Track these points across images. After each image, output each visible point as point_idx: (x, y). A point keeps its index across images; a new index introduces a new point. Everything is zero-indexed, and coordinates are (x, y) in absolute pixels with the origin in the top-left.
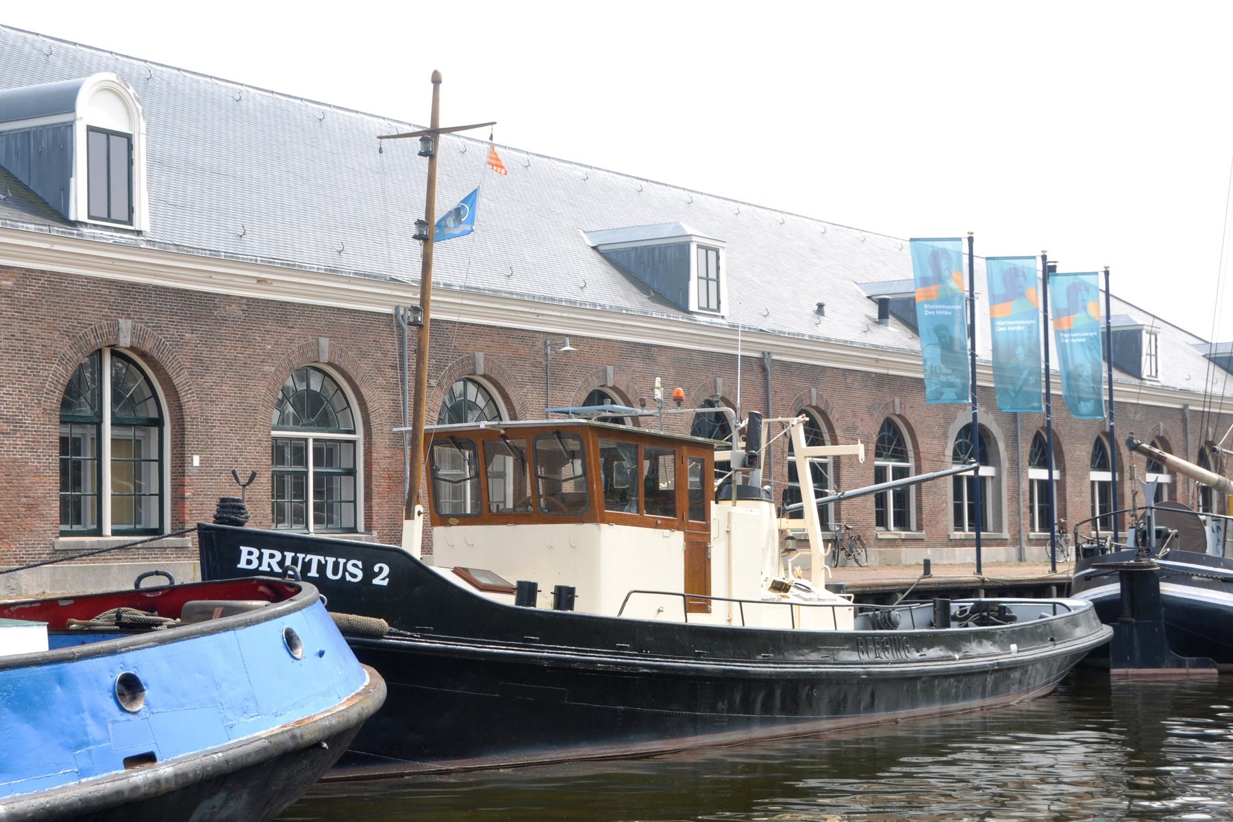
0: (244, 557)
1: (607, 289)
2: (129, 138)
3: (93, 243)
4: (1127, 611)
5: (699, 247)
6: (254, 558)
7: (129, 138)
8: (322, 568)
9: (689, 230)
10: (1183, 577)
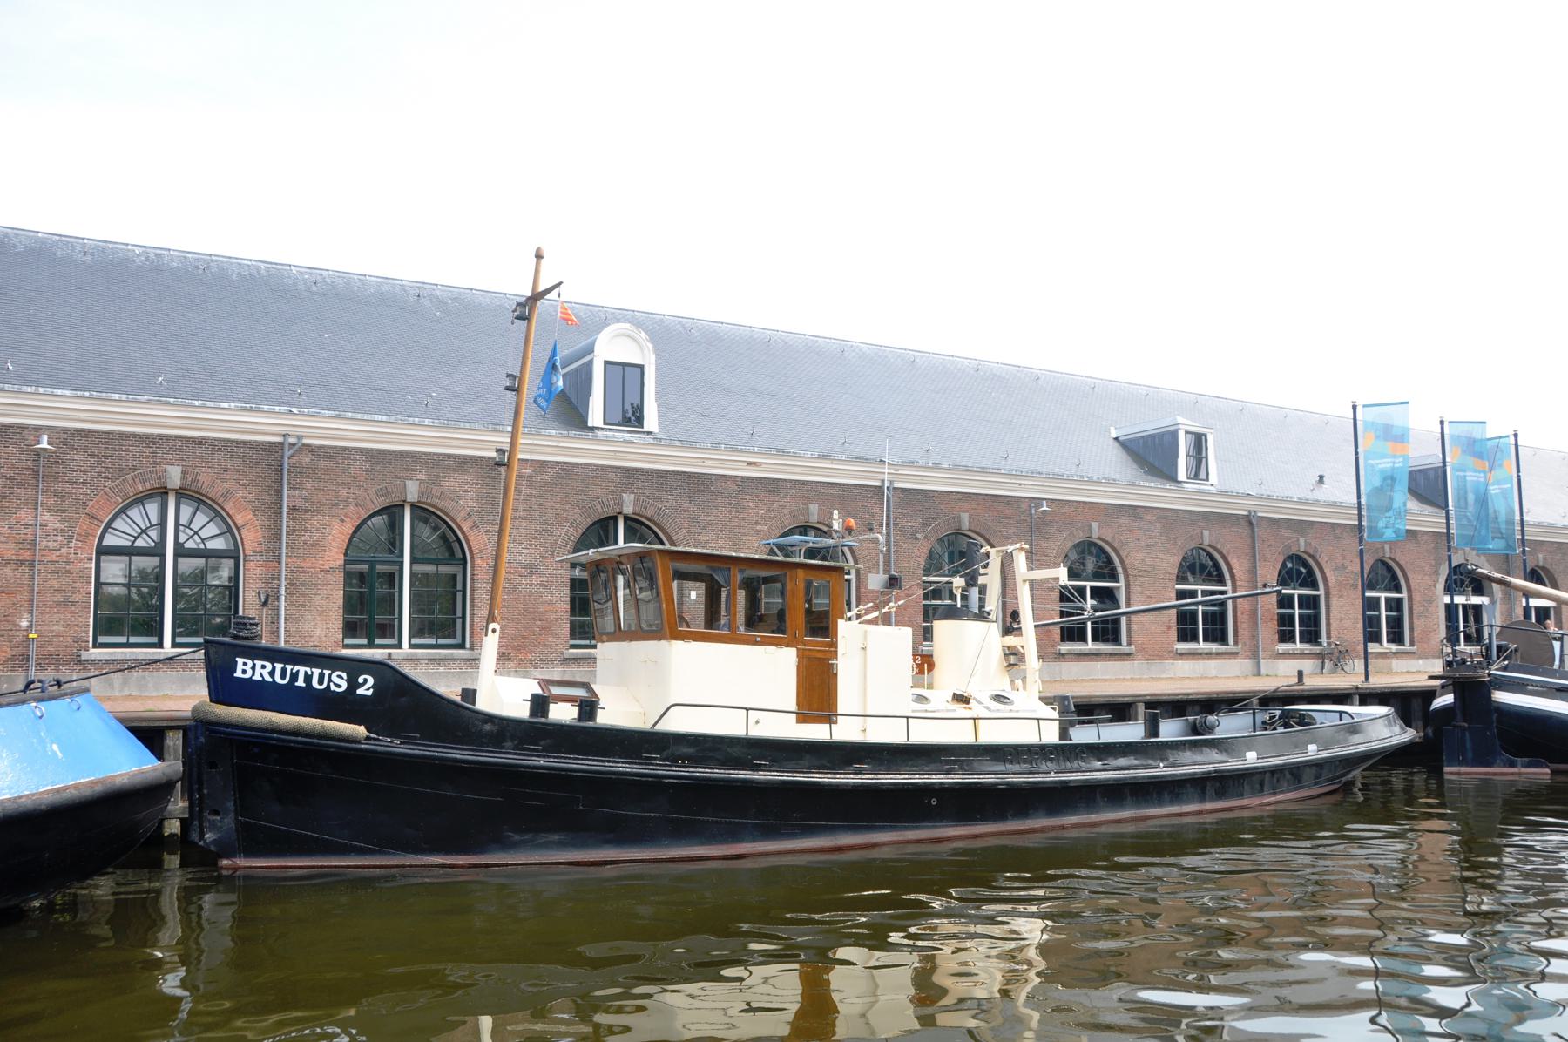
0: (240, 667)
1: (1116, 466)
2: (641, 367)
3: (607, 440)
4: (1459, 716)
6: (248, 668)
7: (641, 367)
8: (308, 678)
10: (1519, 687)
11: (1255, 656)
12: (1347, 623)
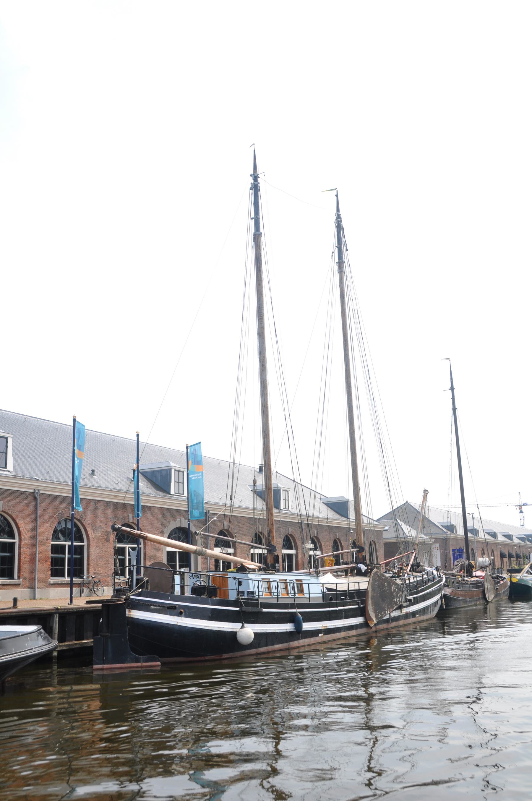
1: (331, 514)
5: (175, 470)
9: (280, 486)
10: (145, 607)
11: (32, 586)
12: (101, 564)
